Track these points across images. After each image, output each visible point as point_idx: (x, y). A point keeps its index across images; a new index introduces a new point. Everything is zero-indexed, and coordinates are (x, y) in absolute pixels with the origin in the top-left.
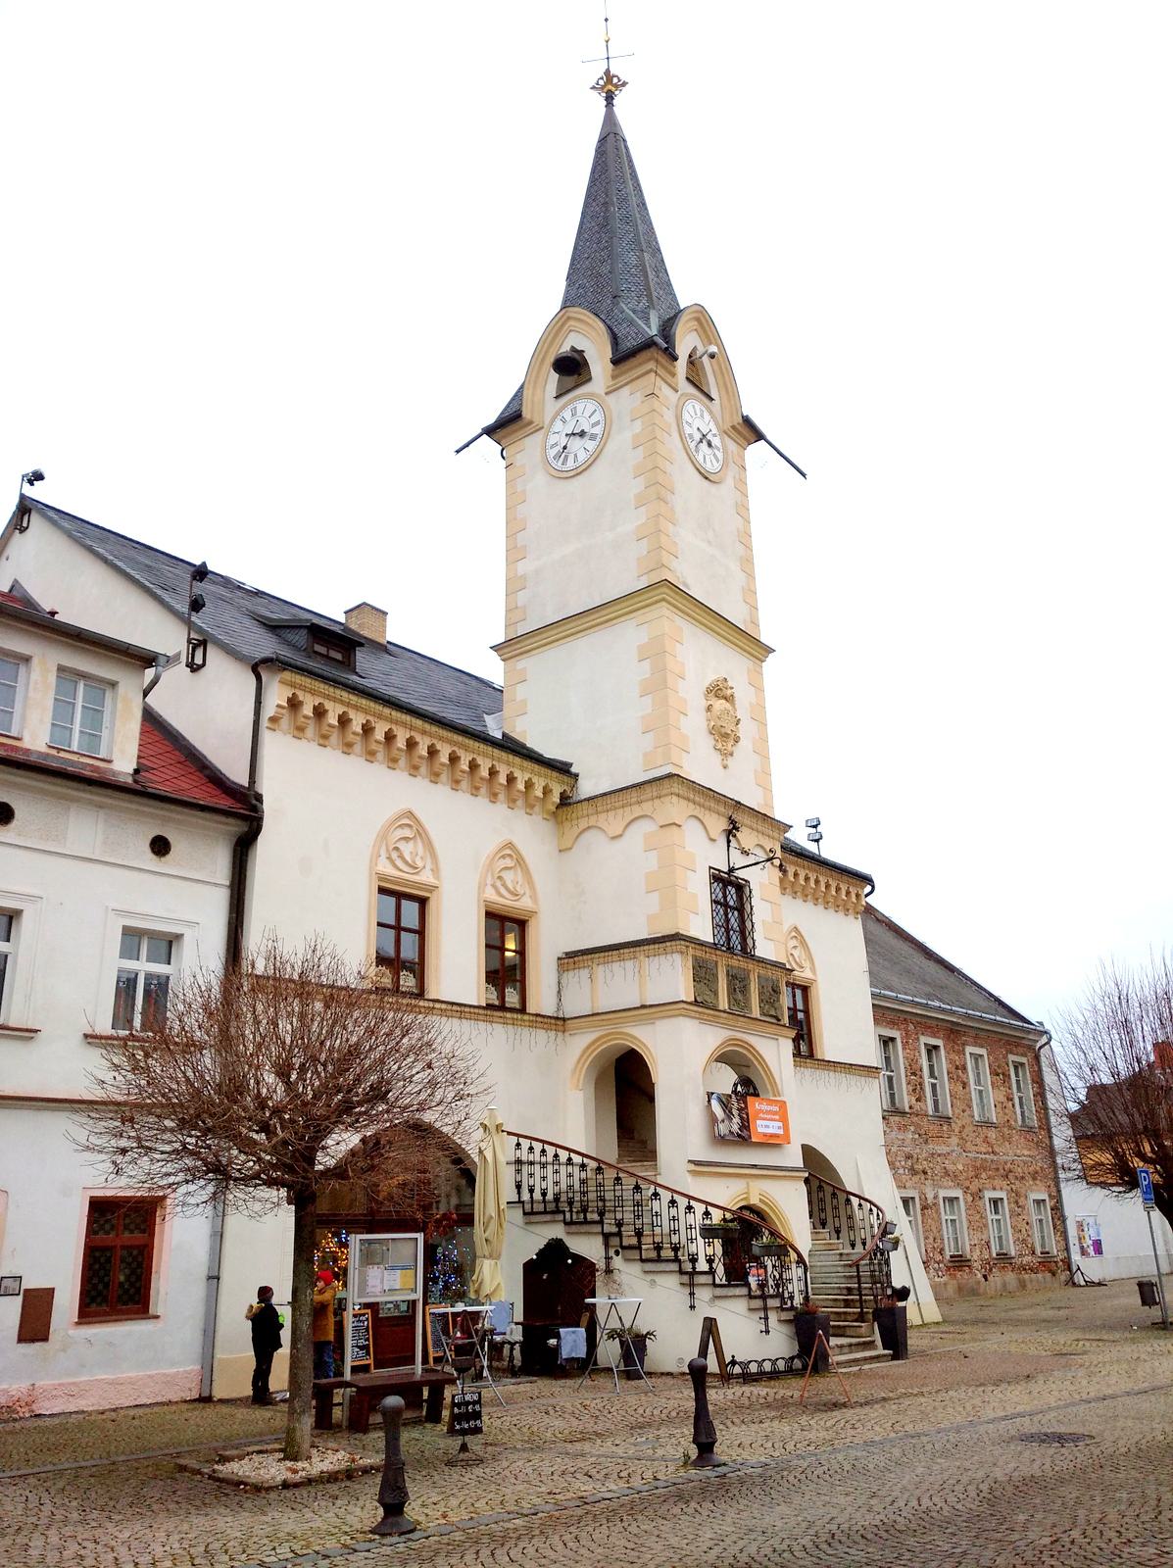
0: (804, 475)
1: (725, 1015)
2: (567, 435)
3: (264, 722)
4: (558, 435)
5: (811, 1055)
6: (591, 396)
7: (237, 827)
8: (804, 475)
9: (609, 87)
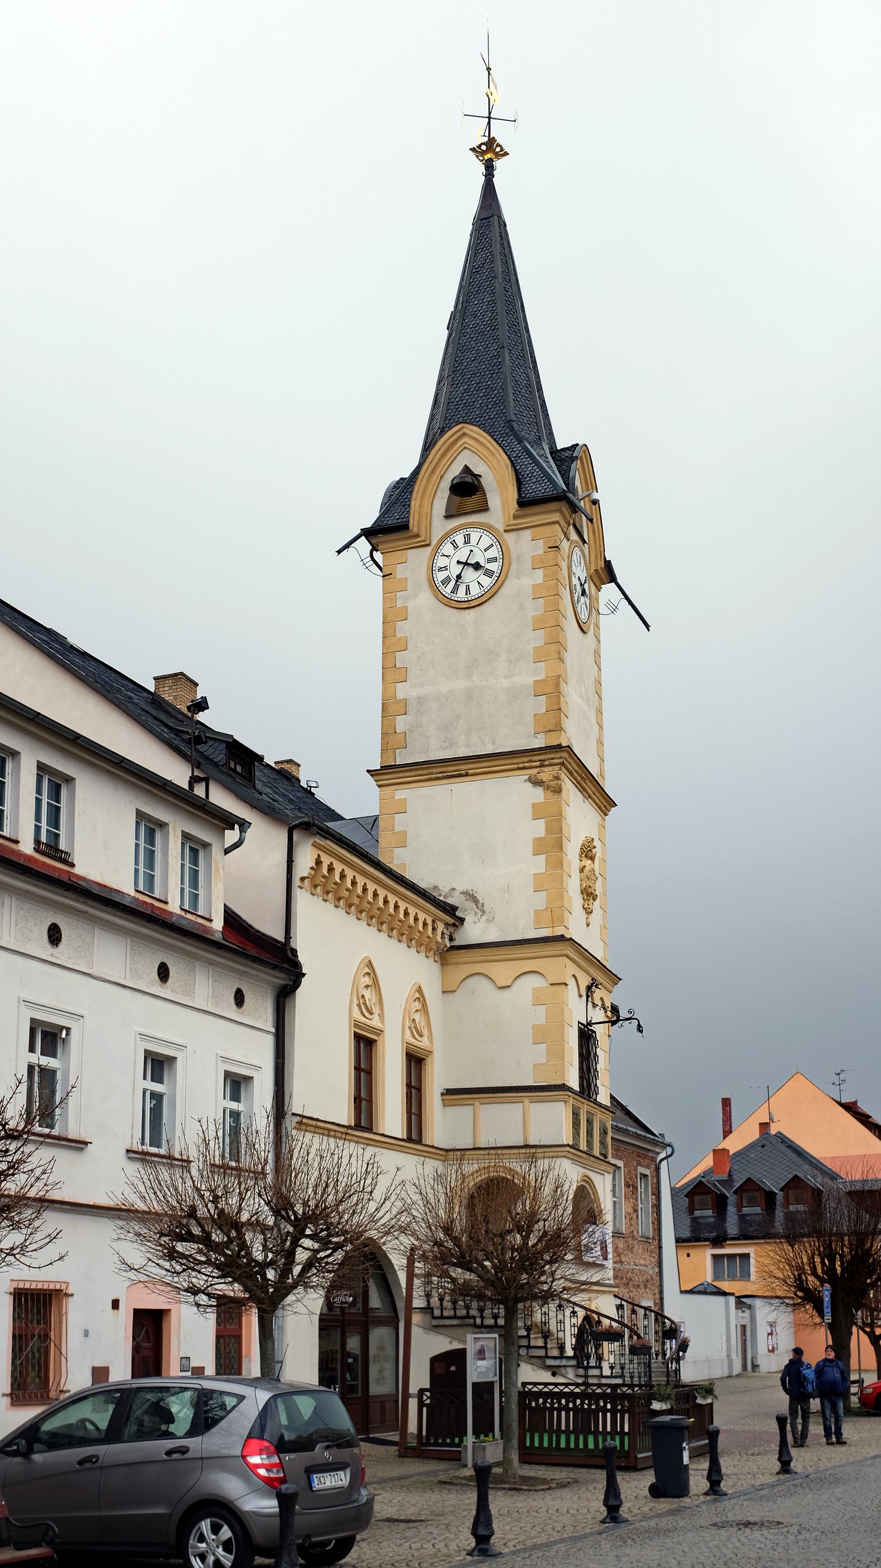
0: (647, 626)
1: (585, 1156)
2: (459, 562)
3: (296, 882)
4: (449, 559)
5: (419, 1142)
6: (488, 528)
7: (280, 979)
8: (647, 626)
9: (489, 152)
